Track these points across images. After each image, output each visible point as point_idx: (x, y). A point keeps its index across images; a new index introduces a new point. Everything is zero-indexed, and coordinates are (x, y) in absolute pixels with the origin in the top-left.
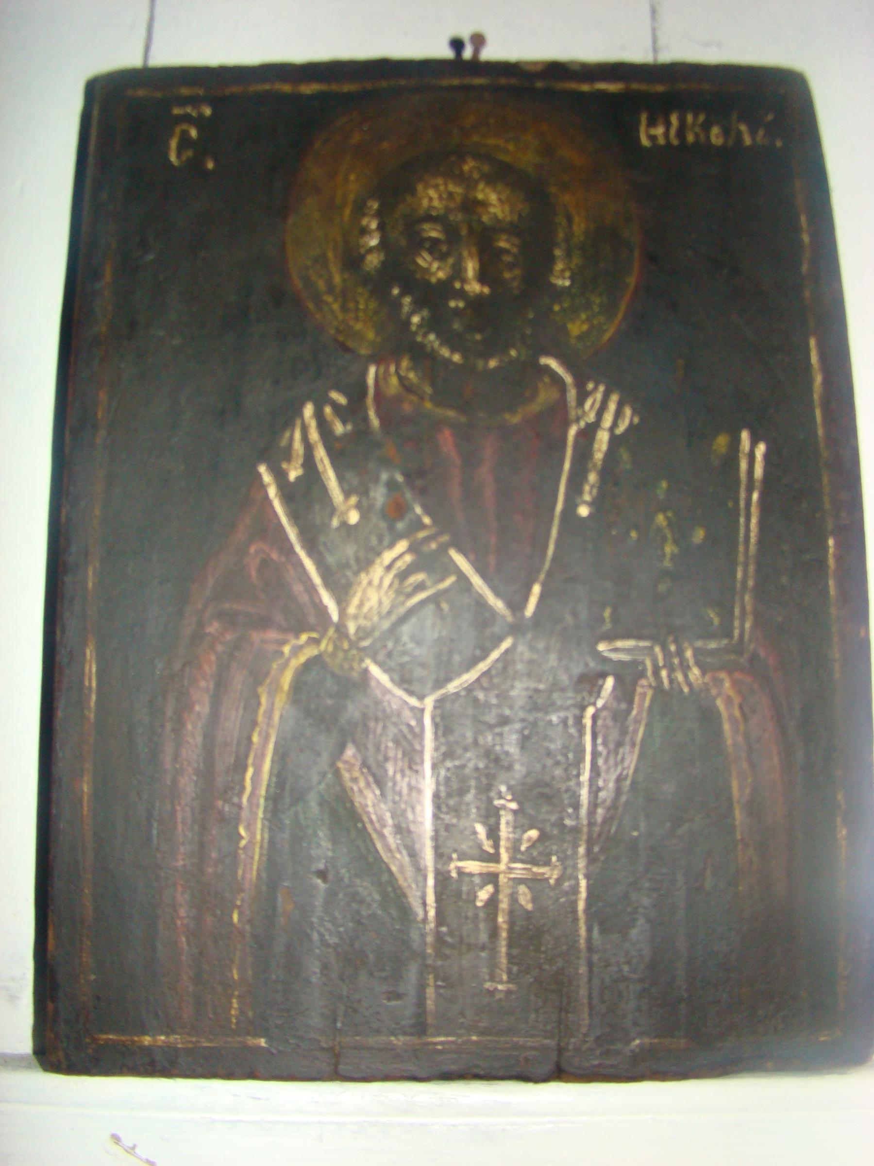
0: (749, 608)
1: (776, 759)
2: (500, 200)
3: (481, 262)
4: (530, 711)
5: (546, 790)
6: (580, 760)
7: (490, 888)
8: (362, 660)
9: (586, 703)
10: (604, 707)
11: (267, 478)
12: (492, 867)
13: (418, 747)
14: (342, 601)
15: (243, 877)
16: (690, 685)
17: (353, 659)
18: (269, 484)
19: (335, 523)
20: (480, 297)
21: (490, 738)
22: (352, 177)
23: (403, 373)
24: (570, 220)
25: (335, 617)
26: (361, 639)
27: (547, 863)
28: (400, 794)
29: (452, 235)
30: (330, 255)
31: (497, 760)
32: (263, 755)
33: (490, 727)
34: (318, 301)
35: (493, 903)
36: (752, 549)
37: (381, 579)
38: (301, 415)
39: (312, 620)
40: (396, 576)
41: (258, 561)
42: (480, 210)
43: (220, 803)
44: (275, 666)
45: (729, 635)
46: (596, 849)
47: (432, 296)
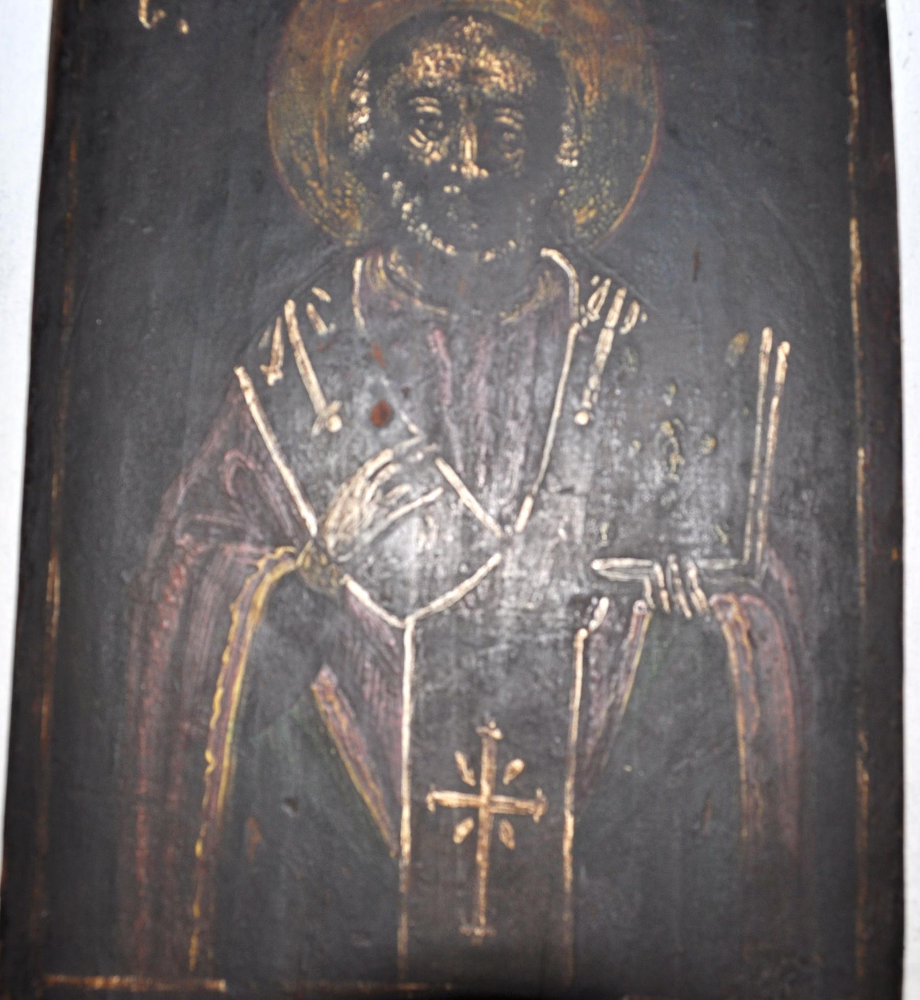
0: (762, 525)
1: (788, 692)
2: (503, 67)
3: (480, 141)
4: (518, 632)
5: (533, 719)
6: (571, 685)
7: (469, 823)
8: (341, 577)
9: (578, 625)
10: (598, 630)
11: (244, 382)
12: (471, 800)
13: (397, 669)
14: (321, 513)
15: (209, 805)
16: (692, 608)
17: (331, 575)
18: (247, 388)
19: (316, 430)
20: (477, 180)
21: (474, 661)
22: (341, 43)
23: (391, 267)
24: (581, 90)
25: (313, 530)
26: (340, 554)
27: (532, 797)
28: (376, 718)
29: (449, 107)
30: (316, 134)
31: (481, 684)
32: (233, 677)
33: (474, 647)
34: (302, 185)
35: (472, 837)
36: (769, 461)
37: (363, 491)
38: (283, 315)
39: (289, 532)
40: (379, 487)
41: (232, 470)
42: (480, 80)
43: (186, 726)
44: (248, 582)
45: (739, 555)
46: (585, 783)
47: (424, 182)
